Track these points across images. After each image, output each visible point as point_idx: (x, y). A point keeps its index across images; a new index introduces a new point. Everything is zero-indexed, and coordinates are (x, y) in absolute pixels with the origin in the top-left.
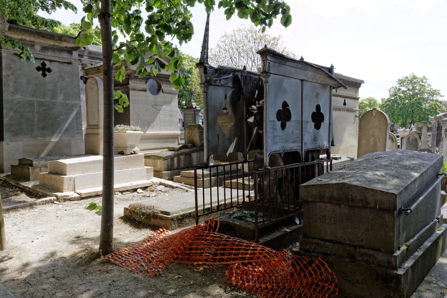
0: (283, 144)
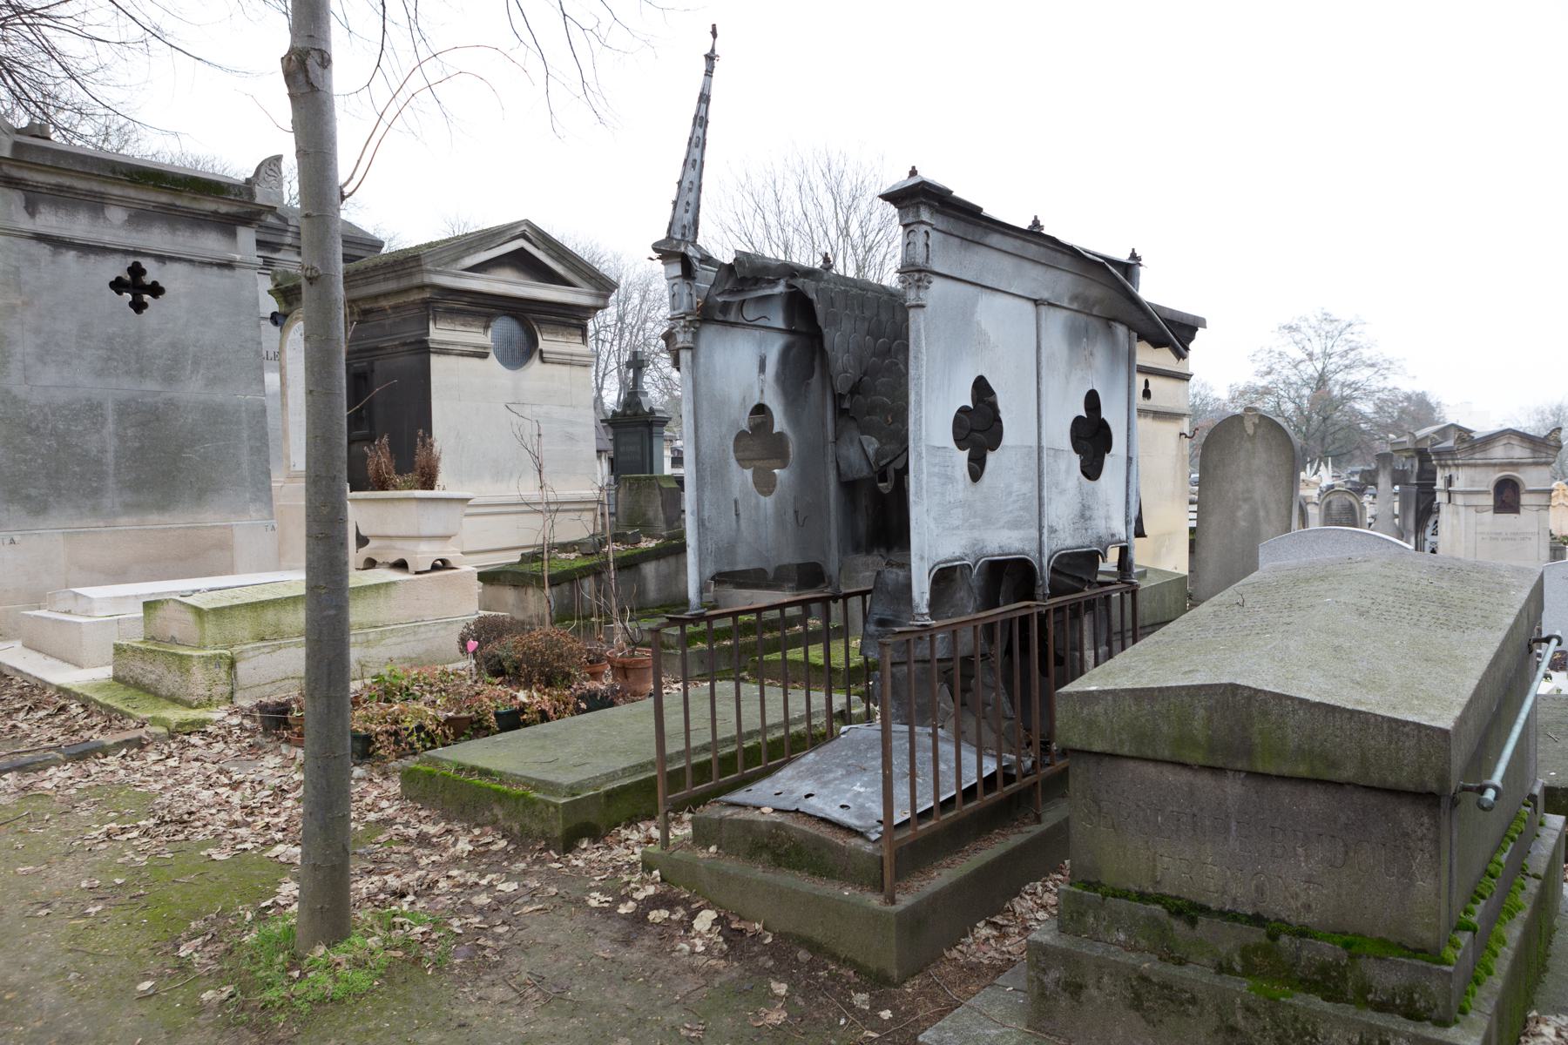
0: (976, 534)
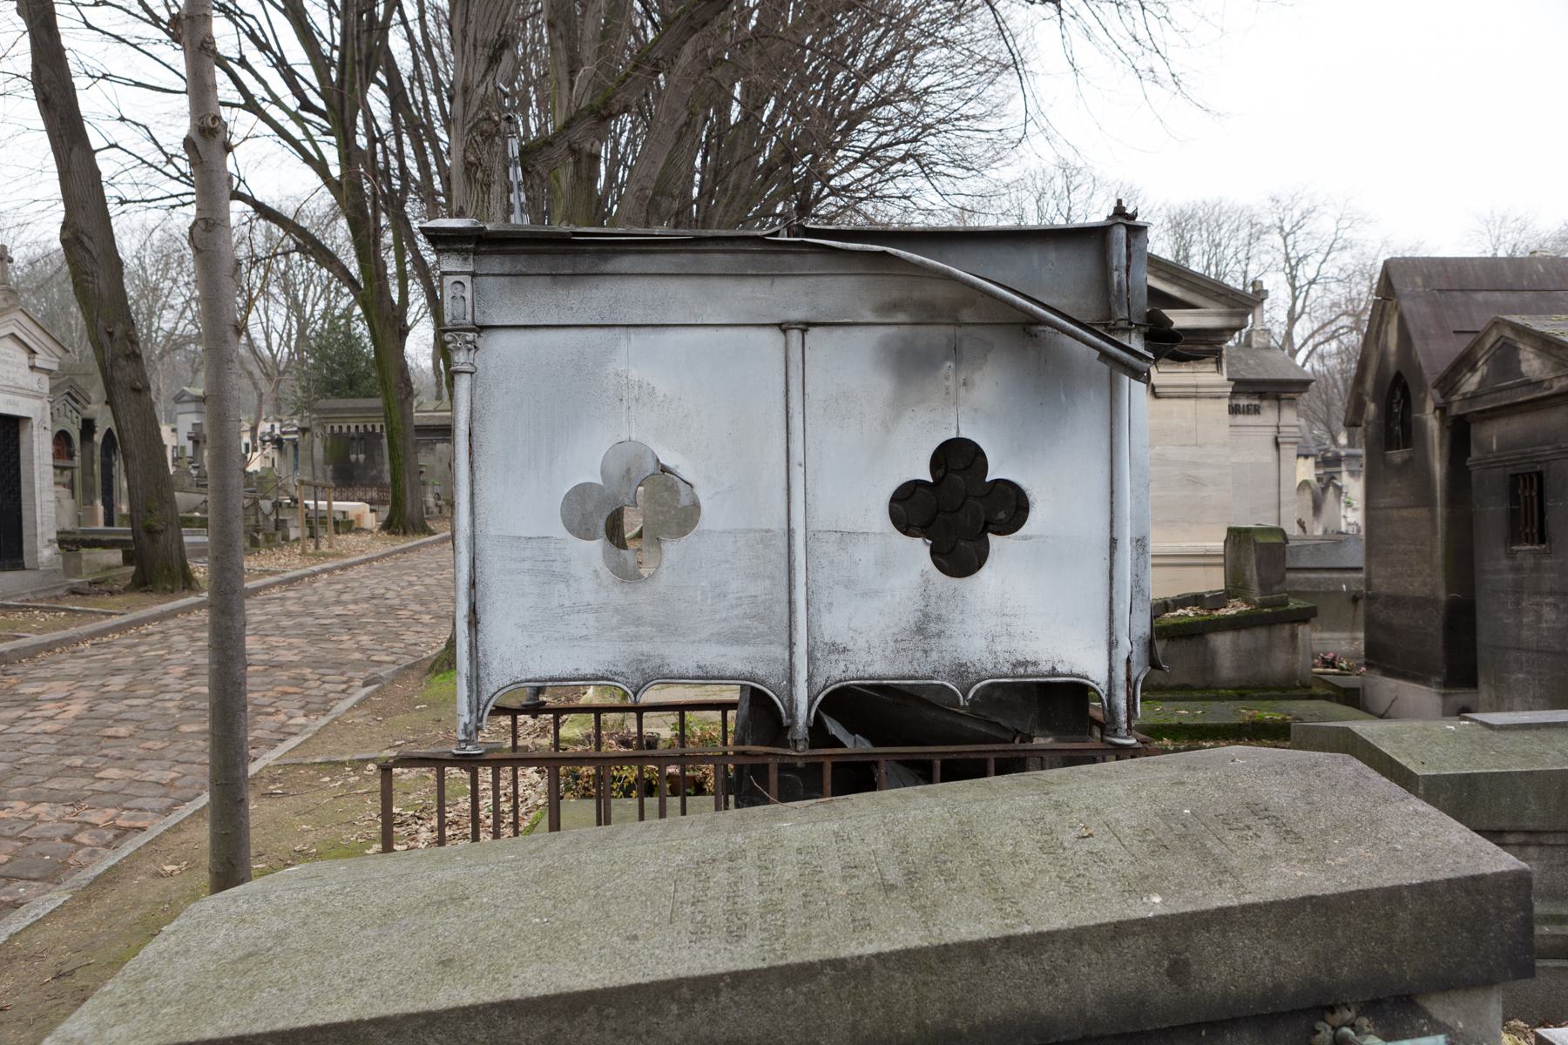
0: (645, 648)
